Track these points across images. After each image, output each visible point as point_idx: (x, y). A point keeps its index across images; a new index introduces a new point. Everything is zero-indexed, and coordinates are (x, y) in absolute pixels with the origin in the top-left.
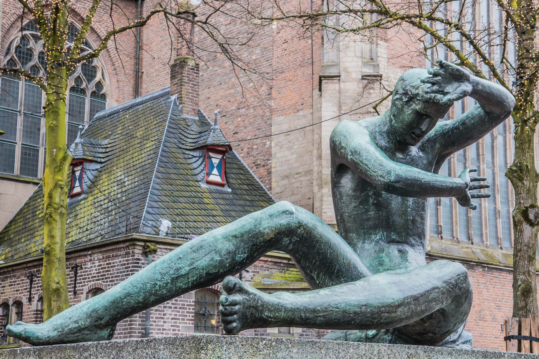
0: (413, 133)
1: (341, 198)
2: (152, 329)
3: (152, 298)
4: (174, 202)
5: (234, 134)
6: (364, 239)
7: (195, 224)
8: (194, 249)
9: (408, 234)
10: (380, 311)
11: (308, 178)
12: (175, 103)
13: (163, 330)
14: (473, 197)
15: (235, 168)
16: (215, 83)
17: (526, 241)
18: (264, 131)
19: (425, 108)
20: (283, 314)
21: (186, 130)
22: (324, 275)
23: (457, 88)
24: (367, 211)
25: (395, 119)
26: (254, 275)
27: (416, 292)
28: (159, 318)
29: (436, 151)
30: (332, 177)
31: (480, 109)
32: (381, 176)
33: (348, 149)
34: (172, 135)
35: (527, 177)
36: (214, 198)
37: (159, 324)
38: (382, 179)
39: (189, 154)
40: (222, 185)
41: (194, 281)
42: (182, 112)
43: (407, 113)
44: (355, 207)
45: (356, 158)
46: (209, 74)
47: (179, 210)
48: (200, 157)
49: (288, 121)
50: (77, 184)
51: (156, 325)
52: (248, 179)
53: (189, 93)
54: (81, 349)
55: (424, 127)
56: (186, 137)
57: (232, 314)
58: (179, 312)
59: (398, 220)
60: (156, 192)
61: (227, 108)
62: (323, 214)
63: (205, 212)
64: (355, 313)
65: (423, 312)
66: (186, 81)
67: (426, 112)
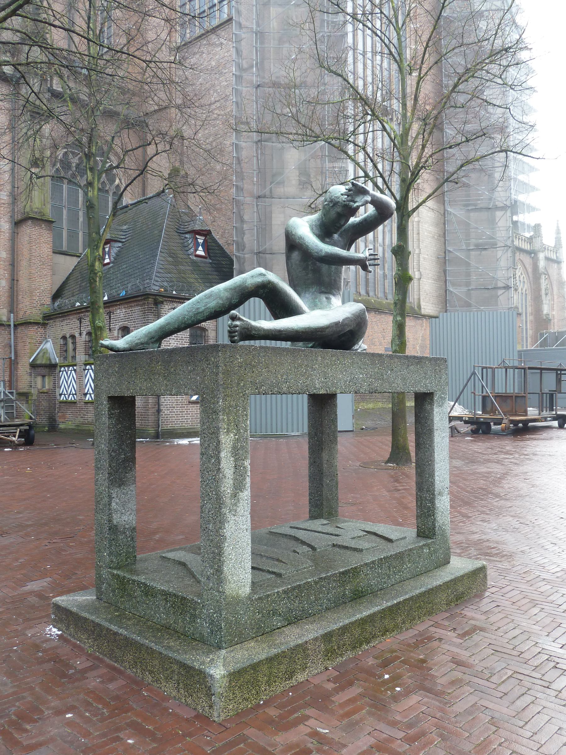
1: (292, 266)
14: (370, 265)
20: (262, 333)
24: (307, 274)
48: (190, 238)
50: (107, 257)
57: (235, 332)
59: (326, 279)
60: (162, 262)
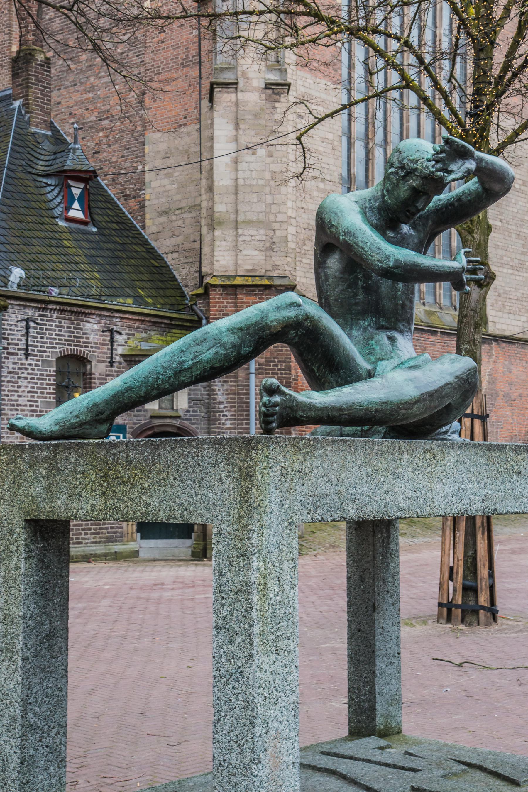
0: (408, 211)
1: (327, 280)
2: (4, 405)
3: (154, 393)
4: (25, 244)
5: (94, 153)
6: (352, 325)
7: (54, 273)
8: (197, 342)
9: (397, 320)
10: (399, 408)
11: (193, 214)
12: (20, 111)
13: (18, 405)
15: (101, 201)
16: (67, 84)
17: (473, 304)
18: (134, 151)
19: (423, 185)
21: (36, 149)
22: (325, 367)
23: (462, 165)
24: (356, 294)
25: (388, 194)
26: (128, 338)
27: (430, 388)
28: (12, 391)
29: (428, 229)
30: (315, 255)
31: (477, 185)
32: (378, 261)
33: (340, 229)
34: (18, 155)
35: (478, 229)
36: (76, 240)
37: (13, 398)
38: (380, 264)
39: (41, 182)
40: (85, 223)
41: (197, 375)
42: (29, 124)
43: (403, 189)
44: (342, 290)
45: (350, 240)
46: (58, 70)
47: (32, 255)
49: (167, 139)
51: (9, 400)
52: (117, 216)
53: (39, 98)
54: (107, 446)
55: (420, 205)
56: (36, 158)
57: (272, 415)
58: (36, 383)
59: (387, 304)
61: (84, 119)
62: (215, 263)
63: (65, 258)
64: (377, 410)
65: (435, 407)
66: (34, 81)
67: (424, 189)
